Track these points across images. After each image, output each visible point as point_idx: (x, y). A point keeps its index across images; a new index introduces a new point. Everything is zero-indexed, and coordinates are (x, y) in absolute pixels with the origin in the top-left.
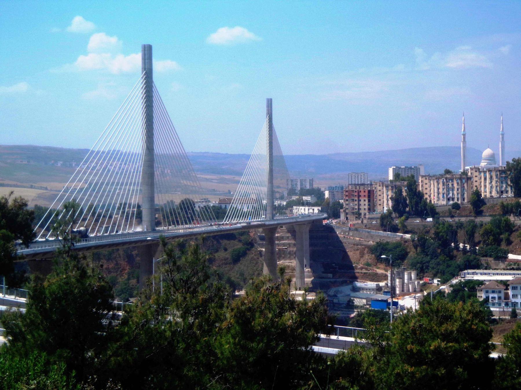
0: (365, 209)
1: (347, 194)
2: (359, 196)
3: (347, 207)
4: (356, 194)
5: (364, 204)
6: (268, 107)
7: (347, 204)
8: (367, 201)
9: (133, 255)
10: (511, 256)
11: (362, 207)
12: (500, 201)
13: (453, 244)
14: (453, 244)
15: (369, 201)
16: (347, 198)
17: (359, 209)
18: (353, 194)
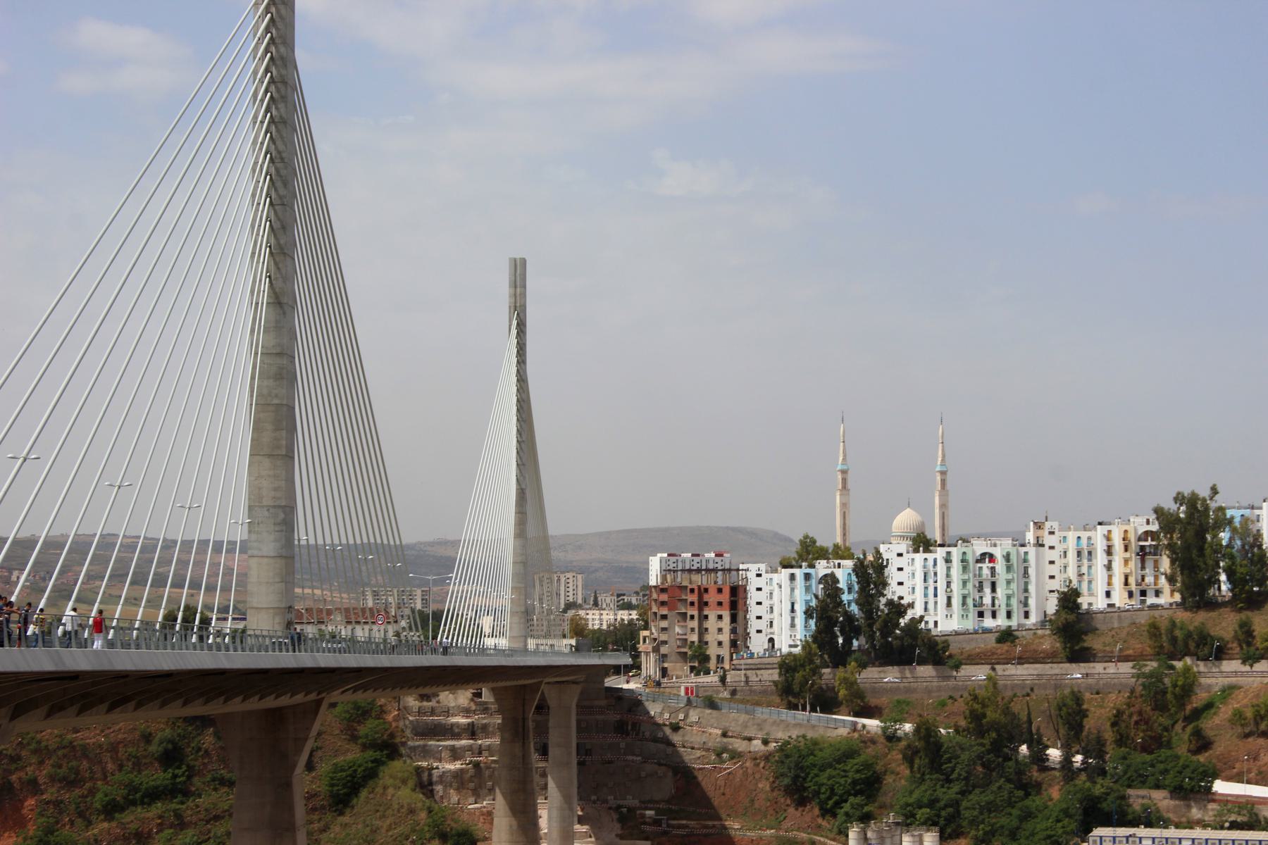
0: (720, 643)
1: (664, 597)
2: (703, 604)
3: (663, 637)
4: (693, 598)
5: (718, 629)
6: (514, 285)
7: (664, 629)
8: (727, 615)
9: (11, 784)
10: (1220, 787)
11: (711, 637)
12: (1143, 618)
13: (1024, 749)
14: (1024, 749)
15: (734, 619)
16: (664, 611)
17: (703, 643)
18: (681, 596)
